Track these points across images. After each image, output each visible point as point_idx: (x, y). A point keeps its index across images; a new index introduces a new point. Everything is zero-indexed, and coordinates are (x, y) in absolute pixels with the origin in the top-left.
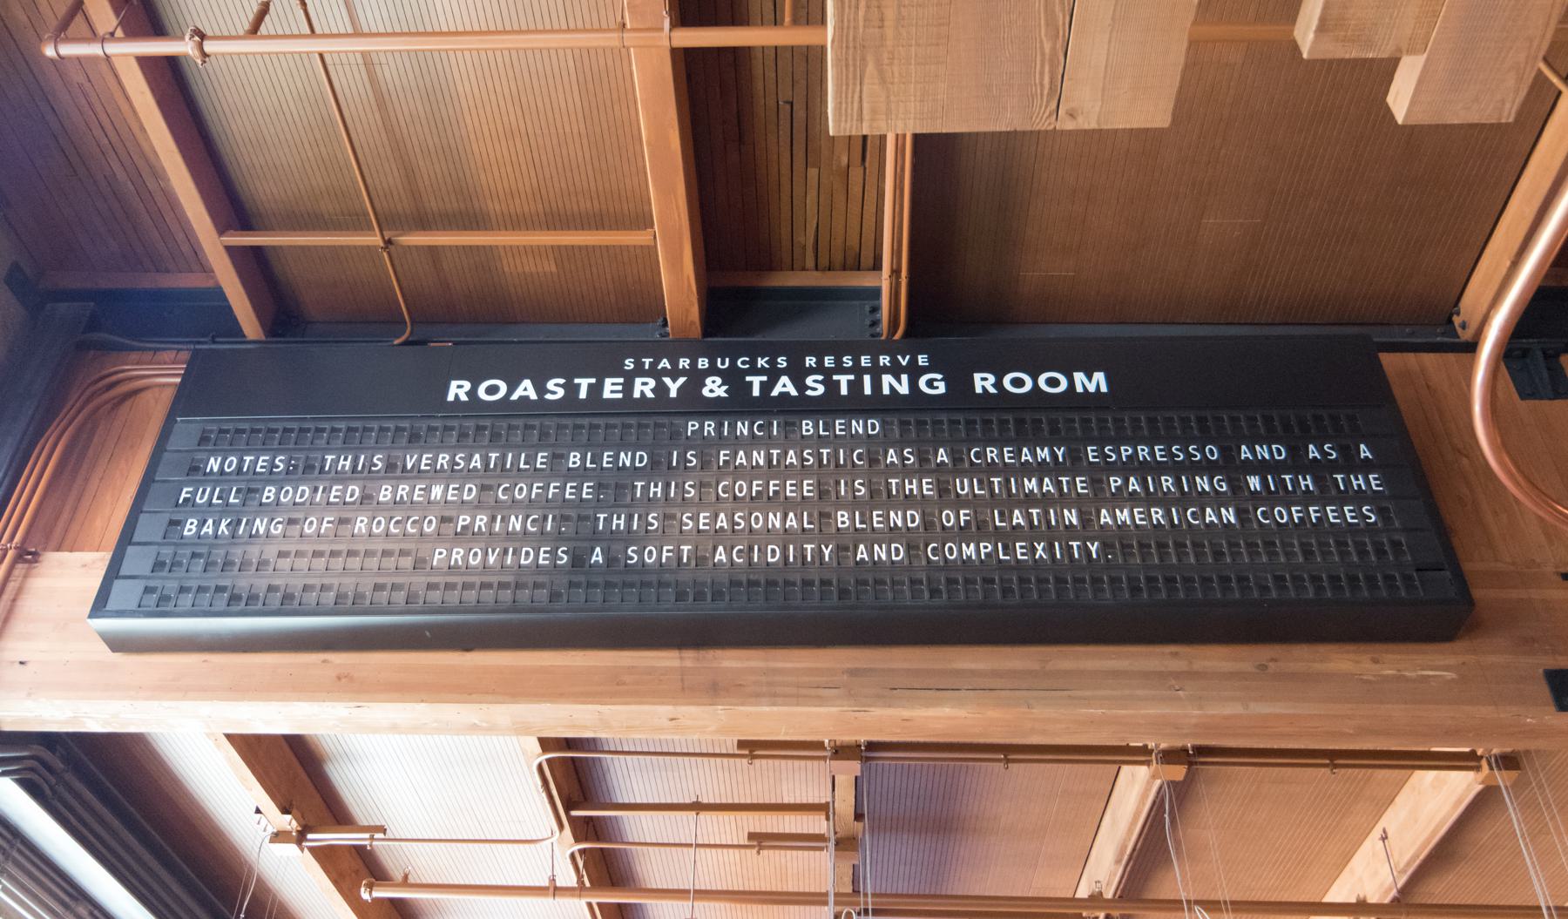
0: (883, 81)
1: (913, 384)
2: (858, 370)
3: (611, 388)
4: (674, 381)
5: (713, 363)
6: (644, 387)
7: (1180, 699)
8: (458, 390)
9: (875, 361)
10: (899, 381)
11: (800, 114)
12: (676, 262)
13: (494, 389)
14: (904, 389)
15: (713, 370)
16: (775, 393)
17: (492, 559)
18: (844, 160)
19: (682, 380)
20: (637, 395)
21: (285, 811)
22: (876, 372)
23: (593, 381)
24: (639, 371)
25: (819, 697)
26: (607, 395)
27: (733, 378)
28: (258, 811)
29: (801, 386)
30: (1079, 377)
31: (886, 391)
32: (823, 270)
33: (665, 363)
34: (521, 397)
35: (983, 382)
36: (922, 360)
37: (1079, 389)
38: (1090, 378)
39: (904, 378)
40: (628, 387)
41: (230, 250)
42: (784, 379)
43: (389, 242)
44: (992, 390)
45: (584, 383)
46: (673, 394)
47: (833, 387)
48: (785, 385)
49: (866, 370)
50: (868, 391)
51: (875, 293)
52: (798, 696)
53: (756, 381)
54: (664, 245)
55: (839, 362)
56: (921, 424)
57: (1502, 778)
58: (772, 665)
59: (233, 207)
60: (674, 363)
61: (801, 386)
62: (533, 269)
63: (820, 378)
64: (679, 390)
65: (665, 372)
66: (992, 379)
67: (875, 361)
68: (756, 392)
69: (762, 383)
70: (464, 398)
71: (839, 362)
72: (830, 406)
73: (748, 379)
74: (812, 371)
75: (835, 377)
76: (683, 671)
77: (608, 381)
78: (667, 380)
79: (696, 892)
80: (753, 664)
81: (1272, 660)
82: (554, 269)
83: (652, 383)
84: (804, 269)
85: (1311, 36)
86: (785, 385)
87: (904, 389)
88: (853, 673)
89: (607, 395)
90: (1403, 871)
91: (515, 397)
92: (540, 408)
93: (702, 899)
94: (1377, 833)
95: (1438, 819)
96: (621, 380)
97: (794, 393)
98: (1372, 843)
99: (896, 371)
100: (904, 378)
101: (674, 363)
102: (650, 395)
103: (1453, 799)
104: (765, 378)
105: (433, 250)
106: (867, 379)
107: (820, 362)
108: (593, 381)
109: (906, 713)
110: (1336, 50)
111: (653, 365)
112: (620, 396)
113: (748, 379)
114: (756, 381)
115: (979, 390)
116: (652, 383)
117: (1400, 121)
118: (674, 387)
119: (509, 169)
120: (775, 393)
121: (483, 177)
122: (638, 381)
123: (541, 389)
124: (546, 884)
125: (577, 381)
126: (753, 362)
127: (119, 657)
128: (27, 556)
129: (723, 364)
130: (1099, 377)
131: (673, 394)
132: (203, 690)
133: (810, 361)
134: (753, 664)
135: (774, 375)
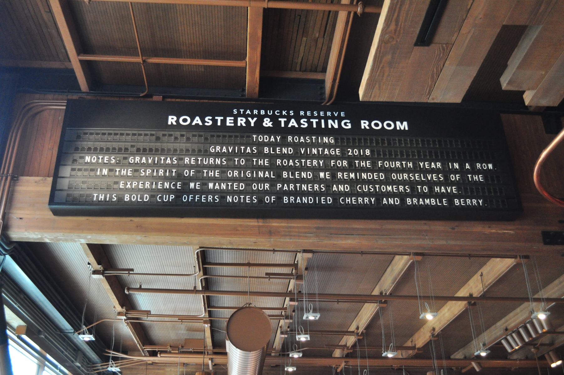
0: (380, 89)
1: (339, 124)
2: (319, 117)
3: (229, 121)
4: (252, 119)
5: (266, 112)
6: (241, 121)
7: (426, 239)
8: (172, 120)
9: (325, 114)
10: (334, 123)
11: (303, 19)
12: (253, 73)
13: (185, 120)
14: (336, 126)
15: (266, 116)
16: (290, 126)
17: (150, 161)
18: (317, 35)
19: (255, 119)
20: (239, 125)
21: (99, 264)
22: (326, 119)
23: (222, 118)
24: (239, 115)
25: (306, 236)
26: (228, 124)
27: (274, 119)
28: (89, 264)
29: (299, 124)
30: (398, 123)
31: (330, 127)
32: (303, 72)
33: (248, 112)
34: (196, 124)
35: (364, 124)
36: (342, 114)
37: (398, 128)
38: (402, 124)
39: (336, 121)
40: (236, 121)
41: (81, 62)
42: (293, 120)
43: (144, 61)
44: (368, 128)
45: (219, 119)
46: (252, 125)
47: (310, 124)
48: (293, 123)
49: (322, 118)
50: (323, 126)
51: (323, 82)
52: (299, 236)
53: (283, 120)
54: (249, 67)
55: (312, 114)
56: (342, 139)
57: (523, 261)
58: (290, 225)
59: (83, 46)
60: (252, 112)
61: (299, 124)
62: (195, 70)
63: (306, 120)
64: (255, 123)
65: (249, 115)
66: (367, 123)
67: (325, 114)
68: (283, 125)
69: (285, 121)
70: (175, 123)
71: (312, 114)
72: (309, 131)
73: (280, 119)
74: (303, 117)
75: (311, 120)
76: (259, 227)
77: (228, 118)
78: (250, 119)
79: (250, 292)
80: (283, 224)
81: (456, 226)
82: (203, 70)
83: (244, 120)
84: (295, 71)
85: (505, 85)
86: (293, 123)
87: (336, 126)
88: (318, 228)
89: (228, 124)
90: (487, 287)
91: (194, 124)
92: (203, 127)
93: (253, 295)
94: (479, 273)
95: (499, 273)
96: (233, 118)
97: (297, 126)
98: (477, 277)
99: (333, 118)
100: (336, 121)
101: (252, 112)
102: (244, 125)
103: (507, 266)
104: (286, 120)
105: (158, 65)
106: (323, 121)
107: (306, 113)
108: (222, 118)
109: (335, 242)
110: (510, 88)
111: (244, 112)
112: (233, 125)
113: (280, 119)
114: (283, 120)
115: (363, 127)
116: (244, 120)
117: (526, 105)
118: (252, 122)
119: (192, 36)
120: (290, 126)
121: (181, 37)
122: (239, 119)
123: (203, 121)
124: (193, 289)
125: (216, 118)
126: (281, 113)
127: (56, 218)
128: (15, 179)
129: (270, 113)
130: (405, 123)
131: (252, 125)
132: (78, 229)
133: (302, 113)
134: (283, 224)
135: (289, 118)
